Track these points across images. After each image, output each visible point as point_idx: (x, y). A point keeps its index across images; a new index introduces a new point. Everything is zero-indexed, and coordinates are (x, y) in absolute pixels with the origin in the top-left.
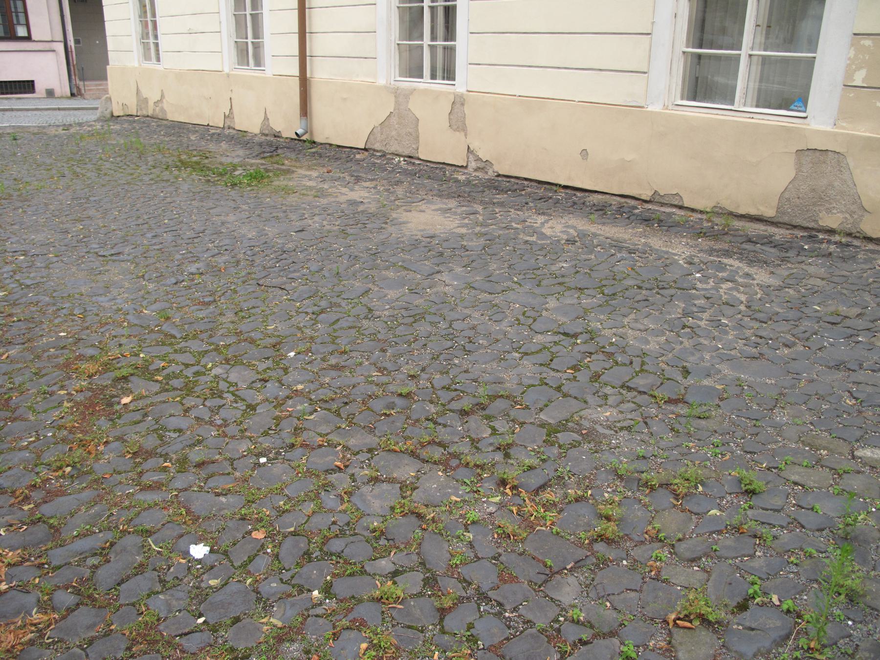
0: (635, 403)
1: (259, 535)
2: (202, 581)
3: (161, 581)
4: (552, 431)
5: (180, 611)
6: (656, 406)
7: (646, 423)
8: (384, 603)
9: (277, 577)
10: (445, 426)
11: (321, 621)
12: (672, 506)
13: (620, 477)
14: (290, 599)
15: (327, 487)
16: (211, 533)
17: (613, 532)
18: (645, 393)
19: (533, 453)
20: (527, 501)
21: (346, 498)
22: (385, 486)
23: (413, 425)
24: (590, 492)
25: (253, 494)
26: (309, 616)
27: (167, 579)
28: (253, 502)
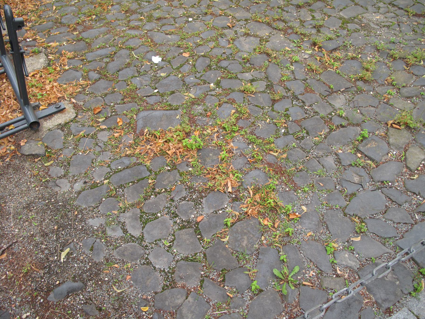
0: (395, 14)
1: (186, 55)
2: (157, 73)
3: (138, 72)
4: (345, 22)
5: (146, 86)
6: (407, 17)
7: (399, 25)
8: (245, 93)
9: (194, 75)
10: (287, 12)
11: (213, 97)
12: (403, 69)
13: (378, 50)
14: (199, 86)
15: (222, 35)
16: (163, 52)
17: (369, 76)
18: (402, 9)
19: (333, 32)
20: (325, 55)
21: (231, 42)
22: (252, 38)
23: (271, 10)
24: (360, 56)
25: (184, 35)
26: (208, 95)
27: (141, 71)
28: (184, 39)
